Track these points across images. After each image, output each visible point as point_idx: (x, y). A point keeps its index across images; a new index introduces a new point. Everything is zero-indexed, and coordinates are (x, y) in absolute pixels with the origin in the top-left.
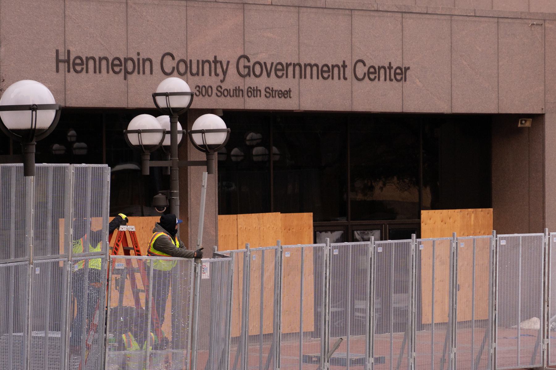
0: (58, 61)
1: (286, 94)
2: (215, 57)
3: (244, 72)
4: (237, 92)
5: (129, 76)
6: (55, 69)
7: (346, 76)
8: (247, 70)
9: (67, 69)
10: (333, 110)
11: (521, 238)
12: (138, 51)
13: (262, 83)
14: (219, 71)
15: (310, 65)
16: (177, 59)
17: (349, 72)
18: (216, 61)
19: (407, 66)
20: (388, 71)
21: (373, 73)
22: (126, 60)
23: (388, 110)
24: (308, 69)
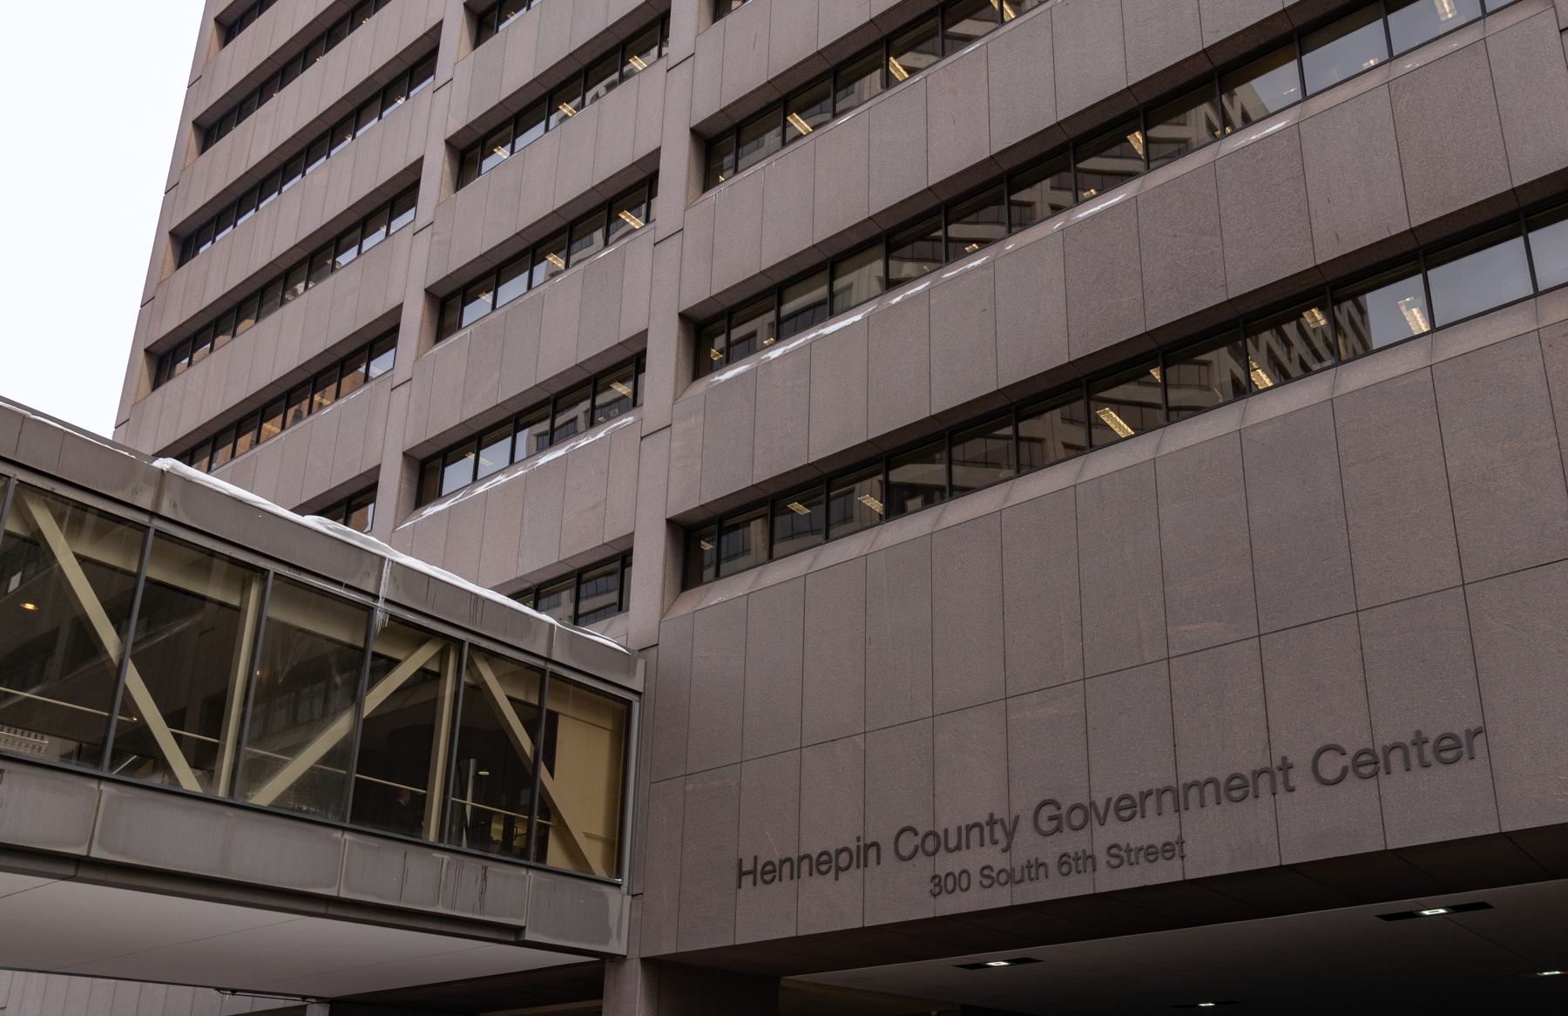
0: (741, 874)
1: (1173, 849)
3: (1046, 826)
5: (841, 874)
11: (13, 483)
16: (921, 834)
21: (1368, 763)
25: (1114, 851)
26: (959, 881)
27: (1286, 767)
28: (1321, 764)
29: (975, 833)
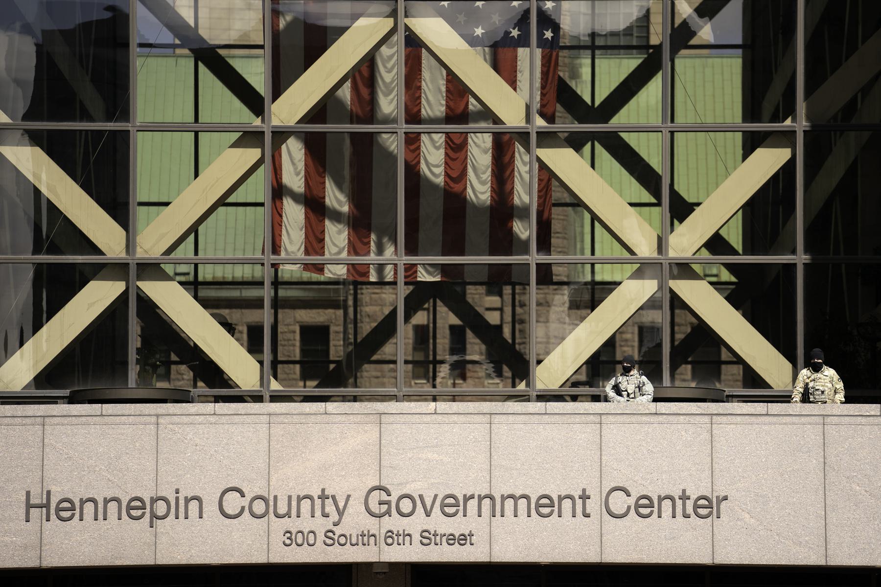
0: (29, 506)
1: (463, 539)
2: (323, 490)
4: (366, 537)
6: (23, 517)
7: (588, 511)
8: (384, 508)
9: (44, 517)
10: (562, 561)
12: (176, 487)
13: (417, 523)
14: (330, 508)
15: (511, 496)
16: (249, 497)
17: (593, 506)
18: (323, 497)
19: (723, 494)
20: (679, 503)
21: (645, 506)
22: (154, 500)
23: (679, 561)
24: (510, 503)
25: (424, 534)
26: (306, 538)
27: (585, 497)
28: (611, 500)
29: (306, 505)
